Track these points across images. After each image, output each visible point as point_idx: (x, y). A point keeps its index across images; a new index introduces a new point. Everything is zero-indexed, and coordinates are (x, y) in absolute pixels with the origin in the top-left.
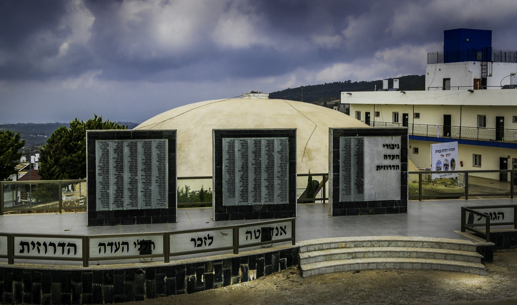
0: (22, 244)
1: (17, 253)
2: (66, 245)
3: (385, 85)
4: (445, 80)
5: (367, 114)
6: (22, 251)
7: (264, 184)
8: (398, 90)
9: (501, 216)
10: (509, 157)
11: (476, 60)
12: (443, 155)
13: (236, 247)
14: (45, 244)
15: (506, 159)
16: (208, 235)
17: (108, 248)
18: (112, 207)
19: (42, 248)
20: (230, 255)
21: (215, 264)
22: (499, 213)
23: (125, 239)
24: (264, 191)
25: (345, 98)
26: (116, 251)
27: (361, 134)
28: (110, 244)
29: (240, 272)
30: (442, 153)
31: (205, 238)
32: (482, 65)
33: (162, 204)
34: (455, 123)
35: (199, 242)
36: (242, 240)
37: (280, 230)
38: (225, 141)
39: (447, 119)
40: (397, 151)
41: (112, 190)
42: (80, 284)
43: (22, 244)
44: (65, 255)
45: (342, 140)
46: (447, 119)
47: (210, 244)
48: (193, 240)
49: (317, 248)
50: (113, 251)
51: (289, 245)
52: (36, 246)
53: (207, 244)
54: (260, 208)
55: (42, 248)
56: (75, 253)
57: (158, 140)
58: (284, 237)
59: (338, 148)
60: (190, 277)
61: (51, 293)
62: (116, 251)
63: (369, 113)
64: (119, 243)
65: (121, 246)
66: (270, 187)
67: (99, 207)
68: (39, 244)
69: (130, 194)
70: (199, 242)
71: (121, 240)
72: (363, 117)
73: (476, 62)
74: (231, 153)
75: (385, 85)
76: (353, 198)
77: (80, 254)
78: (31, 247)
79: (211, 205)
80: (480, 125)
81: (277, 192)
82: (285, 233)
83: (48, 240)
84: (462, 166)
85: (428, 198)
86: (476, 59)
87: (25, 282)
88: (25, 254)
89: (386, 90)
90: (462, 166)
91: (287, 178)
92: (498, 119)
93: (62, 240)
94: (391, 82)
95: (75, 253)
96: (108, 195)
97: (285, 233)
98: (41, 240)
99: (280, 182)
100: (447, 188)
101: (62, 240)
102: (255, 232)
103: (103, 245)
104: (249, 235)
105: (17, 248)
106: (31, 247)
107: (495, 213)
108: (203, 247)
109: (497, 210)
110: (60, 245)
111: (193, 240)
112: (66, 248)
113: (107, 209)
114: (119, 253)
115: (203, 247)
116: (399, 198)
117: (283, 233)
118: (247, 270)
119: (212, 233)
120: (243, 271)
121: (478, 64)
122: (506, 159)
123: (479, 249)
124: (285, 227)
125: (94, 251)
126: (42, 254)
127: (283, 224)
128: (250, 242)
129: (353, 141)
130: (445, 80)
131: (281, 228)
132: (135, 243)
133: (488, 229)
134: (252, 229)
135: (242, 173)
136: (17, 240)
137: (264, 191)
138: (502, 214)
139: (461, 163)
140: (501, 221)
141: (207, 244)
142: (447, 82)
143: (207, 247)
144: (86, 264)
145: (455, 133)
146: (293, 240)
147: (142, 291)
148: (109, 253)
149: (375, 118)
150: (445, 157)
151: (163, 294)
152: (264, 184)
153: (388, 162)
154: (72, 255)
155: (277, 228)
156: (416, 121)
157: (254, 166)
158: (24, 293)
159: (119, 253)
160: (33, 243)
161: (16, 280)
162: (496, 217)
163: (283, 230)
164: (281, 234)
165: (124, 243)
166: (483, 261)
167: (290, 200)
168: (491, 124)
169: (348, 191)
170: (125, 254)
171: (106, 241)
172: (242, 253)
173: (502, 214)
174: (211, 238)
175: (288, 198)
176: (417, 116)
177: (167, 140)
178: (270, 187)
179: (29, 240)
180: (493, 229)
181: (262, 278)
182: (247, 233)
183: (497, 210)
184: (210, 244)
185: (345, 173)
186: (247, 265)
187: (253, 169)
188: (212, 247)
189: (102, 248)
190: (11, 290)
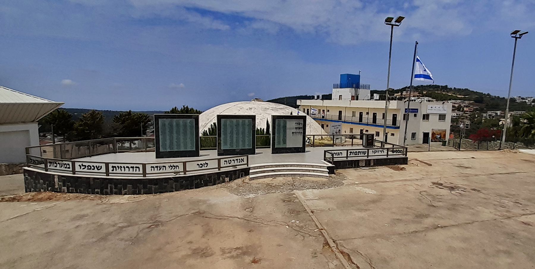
0: (350, 152)
1: (110, 171)
2: (135, 167)
3: (316, 98)
4: (340, 96)
5: (308, 110)
6: (113, 170)
7: (241, 140)
8: (321, 99)
9: (341, 154)
10: (364, 129)
11: (353, 88)
12: (335, 128)
13: (219, 167)
14: (124, 167)
15: (363, 130)
16: (173, 165)
17: (156, 169)
18: (168, 150)
19: (123, 169)
20: (217, 171)
21: (209, 175)
22: (340, 153)
23: (164, 165)
24: (241, 143)
25: (298, 102)
26: (159, 170)
27: (285, 118)
28: (157, 167)
29: (221, 179)
30: (335, 127)
31: (204, 164)
32: (355, 90)
33: (193, 149)
34: (343, 114)
35: (201, 166)
36: (222, 164)
37: (241, 160)
38: (223, 120)
39: (340, 112)
40: (301, 126)
41: (168, 143)
42: (142, 186)
43: (350, 152)
44: (134, 172)
45: (277, 121)
46: (340, 112)
47: (206, 166)
48: (198, 165)
49: (258, 168)
50: (158, 170)
51: (245, 166)
52: (120, 168)
53: (205, 166)
54: (238, 150)
55: (123, 169)
56: (139, 171)
57: (190, 119)
58: (243, 163)
59: (275, 124)
60: (197, 181)
61: (127, 189)
62: (159, 170)
63: (309, 109)
64: (161, 166)
65: (162, 168)
66: (244, 141)
67: (161, 150)
68: (121, 167)
69: (176, 144)
70: (201, 166)
71: (162, 165)
72: (306, 111)
73: (353, 89)
74: (225, 125)
75: (316, 98)
76: (282, 146)
77: (141, 172)
78: (117, 168)
79: (270, 148)
80: (453, 117)
81: (247, 143)
82: (244, 161)
83: (126, 165)
84: (345, 133)
85: (110, 153)
86: (353, 86)
87: (114, 185)
88: (114, 171)
89: (316, 99)
90: (345, 133)
91: (251, 137)
92: (374, 114)
93: (132, 165)
94: (318, 97)
95: (139, 171)
96: (166, 145)
97: (244, 161)
98: (122, 165)
99: (248, 139)
100: (329, 142)
101: (132, 165)
102: (229, 161)
103: (153, 167)
104: (226, 162)
105: (111, 169)
106: (117, 168)
107: (338, 153)
108: (203, 168)
109: (339, 152)
110: (131, 167)
111: (198, 165)
112: (135, 169)
113: (166, 151)
114: (161, 171)
115: (203, 168)
116: (302, 146)
117: (243, 161)
118: (224, 178)
119: (207, 162)
120: (222, 178)
121: (354, 89)
122: (363, 130)
123: (328, 168)
124: (243, 159)
125: (148, 170)
126: (123, 172)
127: (242, 158)
128: (226, 165)
129: (282, 121)
130: (340, 96)
131: (241, 159)
132: (169, 166)
133: (333, 160)
134: (227, 160)
135: (230, 134)
136: (349, 151)
137: (241, 143)
138: (342, 153)
139: (345, 131)
140: (341, 156)
141: (205, 166)
142: (341, 96)
143: (205, 168)
144: (185, 174)
145: (343, 119)
146: (247, 164)
147: (173, 188)
148: (156, 171)
149: (438, 114)
150: (336, 129)
151: (183, 189)
152: (241, 140)
153: (298, 131)
154: (137, 172)
155: (239, 159)
156: (328, 113)
157: (236, 131)
158: (114, 190)
159: (161, 171)
160: (118, 167)
161: (110, 184)
162: (339, 154)
163: (243, 160)
164: (242, 162)
165: (163, 166)
166: (329, 173)
167: (252, 147)
168: (358, 115)
169: (279, 143)
170: (164, 171)
171: (154, 165)
172: (222, 170)
173: (342, 153)
174: (207, 164)
175: (251, 146)
176: (328, 111)
177: (194, 120)
178: (244, 141)
179: (116, 165)
180: (335, 160)
181: (231, 181)
182: (225, 161)
183: (339, 152)
184: (206, 166)
185: (278, 135)
186: (224, 176)
187: (236, 133)
188: (207, 168)
189: (153, 169)
190: (107, 188)
